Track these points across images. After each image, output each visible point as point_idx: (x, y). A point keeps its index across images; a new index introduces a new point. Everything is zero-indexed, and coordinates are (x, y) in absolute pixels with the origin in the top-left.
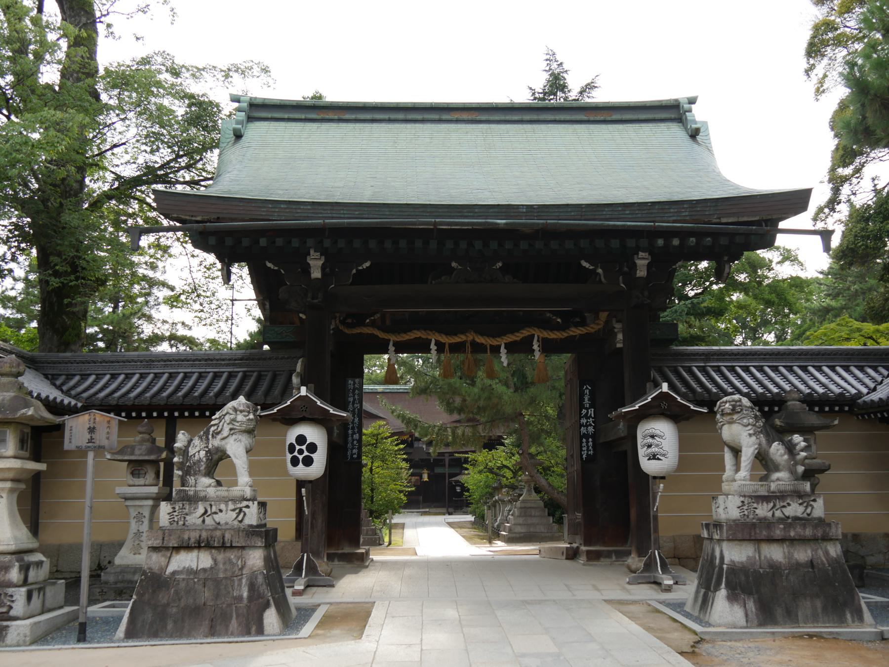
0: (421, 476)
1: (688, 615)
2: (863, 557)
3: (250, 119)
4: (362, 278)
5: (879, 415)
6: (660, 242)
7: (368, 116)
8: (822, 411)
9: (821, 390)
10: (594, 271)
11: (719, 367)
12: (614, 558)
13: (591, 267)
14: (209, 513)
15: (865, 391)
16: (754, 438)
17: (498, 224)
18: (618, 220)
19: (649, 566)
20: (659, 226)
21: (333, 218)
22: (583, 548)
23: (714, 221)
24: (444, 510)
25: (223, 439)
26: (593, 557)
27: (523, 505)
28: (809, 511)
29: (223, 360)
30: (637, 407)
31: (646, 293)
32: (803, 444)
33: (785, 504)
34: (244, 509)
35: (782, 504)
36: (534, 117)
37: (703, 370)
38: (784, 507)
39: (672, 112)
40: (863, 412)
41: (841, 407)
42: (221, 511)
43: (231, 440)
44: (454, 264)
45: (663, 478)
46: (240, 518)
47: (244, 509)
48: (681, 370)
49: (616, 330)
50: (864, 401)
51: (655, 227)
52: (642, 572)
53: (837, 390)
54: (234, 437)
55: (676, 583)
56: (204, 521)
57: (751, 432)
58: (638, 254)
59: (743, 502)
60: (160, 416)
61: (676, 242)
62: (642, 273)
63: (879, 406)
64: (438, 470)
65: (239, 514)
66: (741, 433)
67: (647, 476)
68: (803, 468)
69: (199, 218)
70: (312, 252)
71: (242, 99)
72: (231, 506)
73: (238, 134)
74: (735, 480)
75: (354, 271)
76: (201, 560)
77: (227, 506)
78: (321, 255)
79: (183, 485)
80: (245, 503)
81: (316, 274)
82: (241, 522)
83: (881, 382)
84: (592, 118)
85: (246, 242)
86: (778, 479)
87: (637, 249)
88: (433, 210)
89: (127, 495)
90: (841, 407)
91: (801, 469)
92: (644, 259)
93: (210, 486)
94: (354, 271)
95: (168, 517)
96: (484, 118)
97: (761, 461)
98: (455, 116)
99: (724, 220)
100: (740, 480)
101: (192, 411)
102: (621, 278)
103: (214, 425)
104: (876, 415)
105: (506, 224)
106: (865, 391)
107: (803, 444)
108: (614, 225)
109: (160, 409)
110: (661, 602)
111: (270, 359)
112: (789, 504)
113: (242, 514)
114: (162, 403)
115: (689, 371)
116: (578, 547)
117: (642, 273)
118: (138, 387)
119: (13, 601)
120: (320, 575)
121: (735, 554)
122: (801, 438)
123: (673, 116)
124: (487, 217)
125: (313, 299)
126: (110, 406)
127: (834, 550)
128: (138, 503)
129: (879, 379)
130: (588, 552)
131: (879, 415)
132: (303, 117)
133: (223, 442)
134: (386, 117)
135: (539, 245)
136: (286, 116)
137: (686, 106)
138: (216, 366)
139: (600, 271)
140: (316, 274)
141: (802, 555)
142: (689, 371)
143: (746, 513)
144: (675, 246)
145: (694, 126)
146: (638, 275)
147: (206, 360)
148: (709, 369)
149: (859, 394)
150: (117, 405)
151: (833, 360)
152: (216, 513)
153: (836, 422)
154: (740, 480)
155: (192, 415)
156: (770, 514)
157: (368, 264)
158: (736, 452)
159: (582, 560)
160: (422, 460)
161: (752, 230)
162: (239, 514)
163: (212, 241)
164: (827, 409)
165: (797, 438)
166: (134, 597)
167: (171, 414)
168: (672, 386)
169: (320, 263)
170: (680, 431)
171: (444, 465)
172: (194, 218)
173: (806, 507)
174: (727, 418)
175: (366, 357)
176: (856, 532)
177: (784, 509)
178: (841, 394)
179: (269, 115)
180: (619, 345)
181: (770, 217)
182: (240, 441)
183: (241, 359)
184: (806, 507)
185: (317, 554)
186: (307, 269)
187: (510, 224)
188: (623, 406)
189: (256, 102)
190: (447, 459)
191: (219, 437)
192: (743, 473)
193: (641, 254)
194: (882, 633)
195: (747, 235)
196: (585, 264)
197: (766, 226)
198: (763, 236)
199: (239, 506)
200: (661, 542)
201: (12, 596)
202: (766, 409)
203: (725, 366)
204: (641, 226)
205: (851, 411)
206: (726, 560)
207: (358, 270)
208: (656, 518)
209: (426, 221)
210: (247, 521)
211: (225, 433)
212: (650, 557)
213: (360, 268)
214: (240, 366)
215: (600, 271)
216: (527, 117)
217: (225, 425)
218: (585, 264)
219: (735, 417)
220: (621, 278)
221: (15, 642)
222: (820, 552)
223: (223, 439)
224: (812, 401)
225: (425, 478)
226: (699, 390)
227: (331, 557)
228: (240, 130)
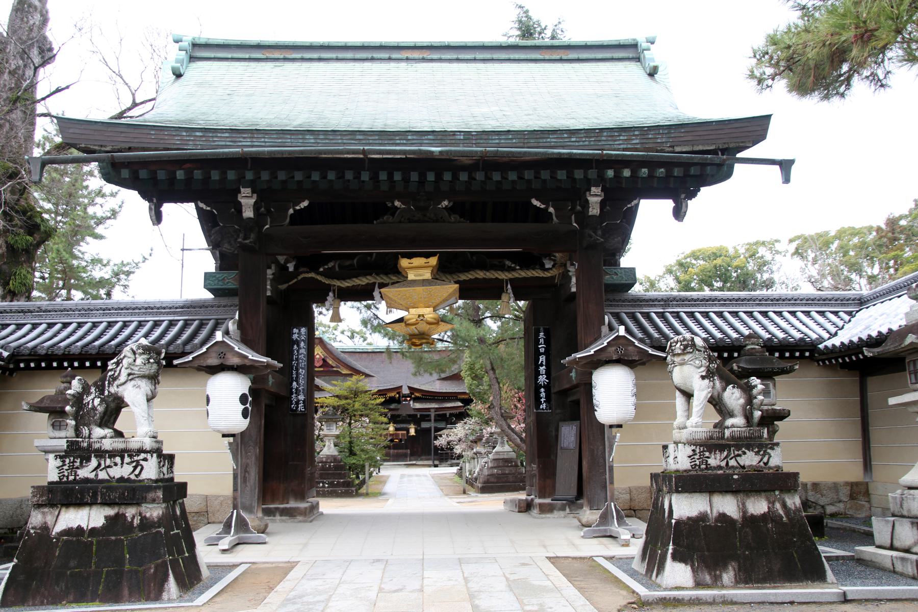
0: (408, 430)
1: (633, 574)
2: (823, 507)
3: (192, 59)
4: (300, 218)
5: (840, 360)
6: (610, 173)
7: (315, 55)
8: (782, 357)
9: (781, 335)
10: (546, 209)
11: (678, 313)
12: (568, 510)
13: (543, 206)
14: (103, 466)
15: (826, 336)
16: (707, 381)
17: (432, 152)
18: (563, 147)
19: (605, 519)
20: (607, 154)
21: (252, 146)
22: (538, 501)
23: (668, 149)
24: (430, 462)
26: (544, 509)
27: (497, 457)
28: (765, 460)
29: (164, 308)
30: (592, 352)
31: (599, 232)
32: (760, 387)
33: (740, 452)
34: (142, 462)
35: (736, 453)
36: (488, 55)
37: (662, 315)
38: (739, 455)
39: (628, 51)
40: (824, 357)
41: (802, 352)
42: (116, 464)
43: (130, 385)
45: (620, 426)
46: (137, 472)
47: (142, 462)
48: (639, 316)
49: (570, 274)
50: (826, 347)
51: (602, 155)
52: (597, 526)
53: (798, 335)
54: (133, 382)
55: (633, 536)
56: (97, 475)
57: (704, 374)
58: (590, 190)
59: (693, 451)
61: (627, 173)
62: (594, 210)
63: (840, 351)
64: (425, 425)
65: (135, 468)
66: (689, 373)
67: (603, 425)
68: (760, 413)
69: (108, 149)
71: (184, 39)
72: (127, 459)
73: (177, 73)
74: (685, 427)
76: (90, 518)
77: (122, 459)
78: (253, 192)
79: (77, 436)
80: (143, 456)
81: (248, 213)
82: (136, 476)
83: (842, 328)
84: (547, 57)
85: (249, 175)
86: (733, 426)
87: (588, 184)
89: (47, 448)
90: (802, 352)
91: (757, 414)
92: (596, 195)
93: (105, 437)
94: (291, 211)
95: (57, 471)
96: (435, 56)
97: (715, 406)
99: (678, 149)
100: (692, 427)
102: (573, 217)
103: (111, 370)
104: (837, 361)
105: (441, 152)
106: (826, 336)
107: (760, 387)
108: (560, 154)
110: (610, 559)
111: (212, 307)
112: (744, 453)
113: (139, 468)
114: (94, 352)
115: (647, 316)
116: (532, 500)
117: (594, 210)
120: (252, 533)
121: (685, 507)
122: (759, 381)
123: (631, 56)
124: (421, 144)
125: (245, 239)
126: (39, 355)
127: (874, 233)
129: (840, 323)
130: (540, 505)
131: (840, 360)
132: (247, 56)
133: (121, 389)
134: (334, 55)
135: (480, 176)
136: (230, 56)
137: (645, 45)
138: (157, 314)
139: (551, 210)
140: (248, 213)
141: (758, 506)
142: (647, 316)
143: (697, 462)
144: (626, 178)
145: (652, 64)
146: (590, 214)
147: (146, 309)
148: (668, 315)
149: (821, 340)
150: (46, 354)
152: (109, 467)
153: (797, 367)
154: (692, 427)
156: (723, 464)
157: (305, 204)
158: (688, 395)
159: (535, 512)
160: (409, 416)
161: (707, 159)
162: (135, 468)
163: (125, 173)
164: (787, 354)
165: (755, 381)
166: (15, 560)
168: (628, 330)
169: (252, 201)
170: (637, 378)
171: (430, 420)
172: (103, 149)
173: (764, 455)
174: (677, 359)
176: (816, 480)
177: (738, 458)
178: (801, 339)
179: (212, 55)
180: (574, 289)
181: (726, 146)
182: (139, 387)
183: (182, 308)
185: (249, 510)
186: (239, 208)
187: (447, 152)
188: (577, 351)
189: (198, 42)
190: (433, 415)
191: (117, 383)
192: (695, 419)
193: (594, 190)
194: (844, 594)
195: (703, 165)
196: (535, 202)
197: (723, 154)
198: (720, 165)
199: (136, 458)
200: (616, 493)
202: (726, 355)
204: (587, 154)
205: (811, 357)
206: (676, 515)
207: (295, 210)
208: (611, 468)
210: (144, 476)
211: (123, 378)
212: (607, 508)
213: (298, 208)
214: (181, 314)
215: (551, 210)
216: (479, 56)
217: (123, 369)
218: (535, 202)
219: (687, 357)
220: (573, 217)
222: (778, 506)
224: (771, 346)
225: (412, 432)
226: (656, 335)
227: (268, 512)
228: (179, 69)
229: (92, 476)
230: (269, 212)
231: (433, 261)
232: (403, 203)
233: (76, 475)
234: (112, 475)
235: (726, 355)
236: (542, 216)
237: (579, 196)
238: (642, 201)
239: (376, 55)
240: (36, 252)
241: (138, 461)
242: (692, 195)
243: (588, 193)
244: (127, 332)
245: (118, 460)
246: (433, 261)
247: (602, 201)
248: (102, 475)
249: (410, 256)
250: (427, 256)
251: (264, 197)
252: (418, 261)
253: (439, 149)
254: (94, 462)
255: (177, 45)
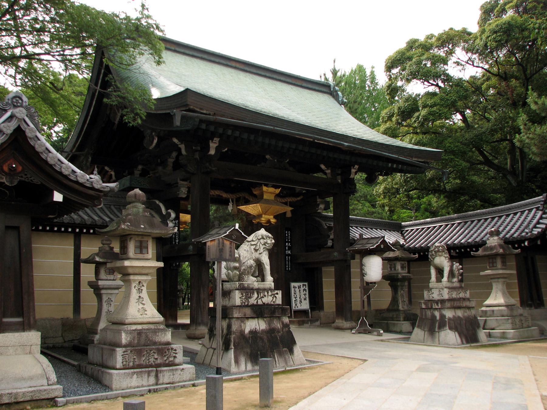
7: (191, 53)
25: (260, 254)
44: (268, 157)
56: (257, 302)
60: (66, 231)
69: (205, 112)
72: (270, 293)
85: (221, 131)
95: (240, 300)
98: (234, 64)
105: (348, 146)
118: (111, 213)
119: (176, 353)
128: (109, 291)
133: (260, 256)
151: (356, 224)
152: (263, 297)
155: (66, 231)
157: (226, 149)
172: (202, 111)
184: (273, 298)
201: (175, 350)
202: (77, 230)
209: (309, 137)
221: (188, 378)
223: (260, 254)
229: (255, 303)
231: (278, 191)
233: (248, 302)
234: (264, 301)
239: (178, 49)
240: (92, 158)
241: (274, 295)
245: (266, 293)
246: (278, 191)
247: (217, 147)
248: (260, 302)
249: (266, 185)
250: (276, 187)
252: (271, 190)
253: (347, 144)
254: (256, 295)
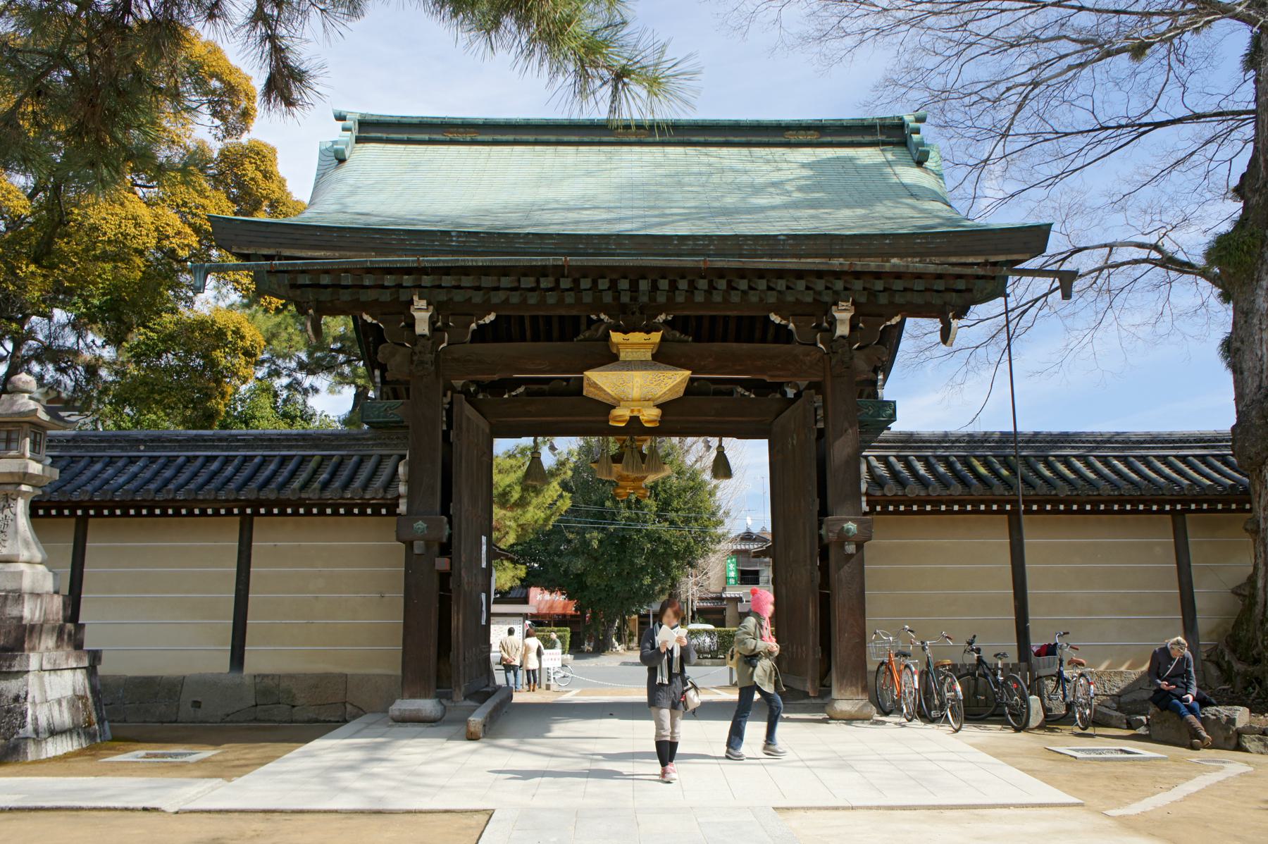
4: (482, 334)
70: (416, 298)
75: (474, 326)
78: (429, 304)
88: (263, 229)
94: (474, 326)
101: (1227, 503)
109: (73, 506)
117: (843, 330)
138: (207, 448)
139: (791, 326)
140: (422, 328)
167: (242, 513)
169: (426, 315)
175: (766, 441)
186: (411, 324)
202: (249, 511)
203: (1155, 457)
207: (478, 326)
213: (481, 322)
215: (791, 326)
230: (446, 325)
232: (610, 317)
235: (79, 512)
236: (782, 335)
237: (823, 309)
238: (910, 322)
242: (961, 313)
243: (834, 308)
244: (286, 472)
251: (439, 308)
255: (340, 124)
